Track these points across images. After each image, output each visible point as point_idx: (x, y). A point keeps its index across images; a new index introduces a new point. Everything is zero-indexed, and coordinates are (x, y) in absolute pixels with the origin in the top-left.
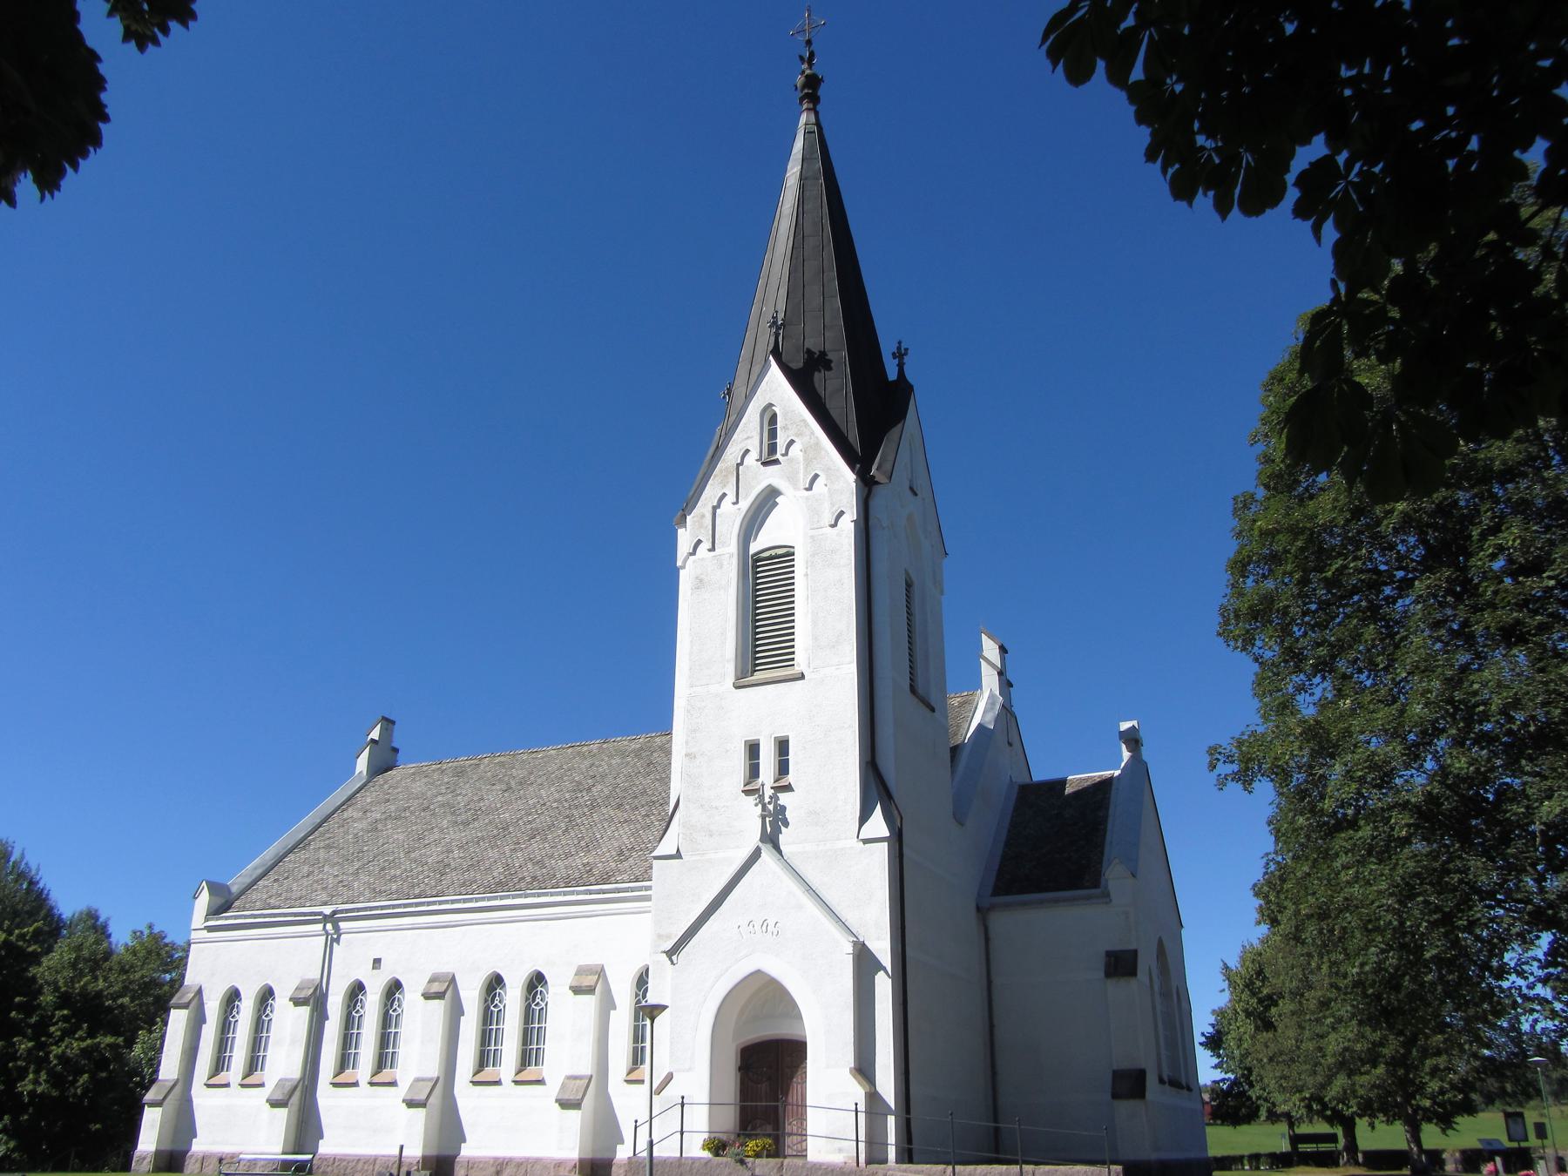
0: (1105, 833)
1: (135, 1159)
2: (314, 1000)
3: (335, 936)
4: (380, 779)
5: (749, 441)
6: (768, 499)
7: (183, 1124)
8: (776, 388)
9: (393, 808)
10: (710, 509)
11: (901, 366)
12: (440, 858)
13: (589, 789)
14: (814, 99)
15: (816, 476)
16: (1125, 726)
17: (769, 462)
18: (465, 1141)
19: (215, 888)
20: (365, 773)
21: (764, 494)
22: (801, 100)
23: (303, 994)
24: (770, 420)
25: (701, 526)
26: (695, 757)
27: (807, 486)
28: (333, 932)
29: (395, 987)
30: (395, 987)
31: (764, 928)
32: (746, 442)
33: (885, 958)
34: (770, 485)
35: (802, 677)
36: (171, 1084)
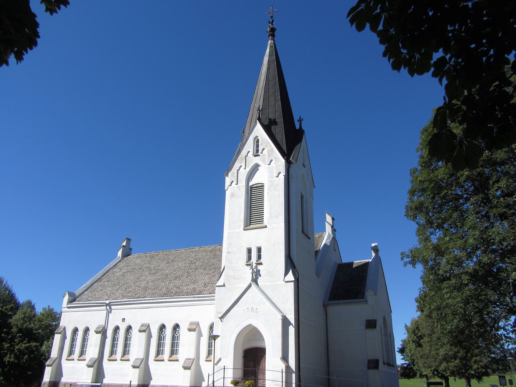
0: (366, 280)
1: (42, 384)
2: (103, 332)
3: (110, 311)
4: (126, 259)
5: (250, 148)
6: (256, 168)
7: (59, 372)
8: (259, 131)
9: (130, 268)
10: (237, 171)
11: (300, 124)
12: (145, 285)
13: (195, 263)
14: (273, 36)
15: (272, 160)
16: (373, 245)
17: (256, 155)
18: (152, 380)
19: (70, 294)
20: (121, 256)
21: (254, 167)
22: (269, 36)
23: (99, 330)
24: (257, 141)
25: (233, 176)
26: (230, 253)
27: (269, 164)
28: (109, 309)
29: (129, 328)
30: (129, 328)
31: (252, 310)
32: (248, 148)
33: (292, 321)
34: (256, 163)
35: (266, 227)
36: (55, 359)
